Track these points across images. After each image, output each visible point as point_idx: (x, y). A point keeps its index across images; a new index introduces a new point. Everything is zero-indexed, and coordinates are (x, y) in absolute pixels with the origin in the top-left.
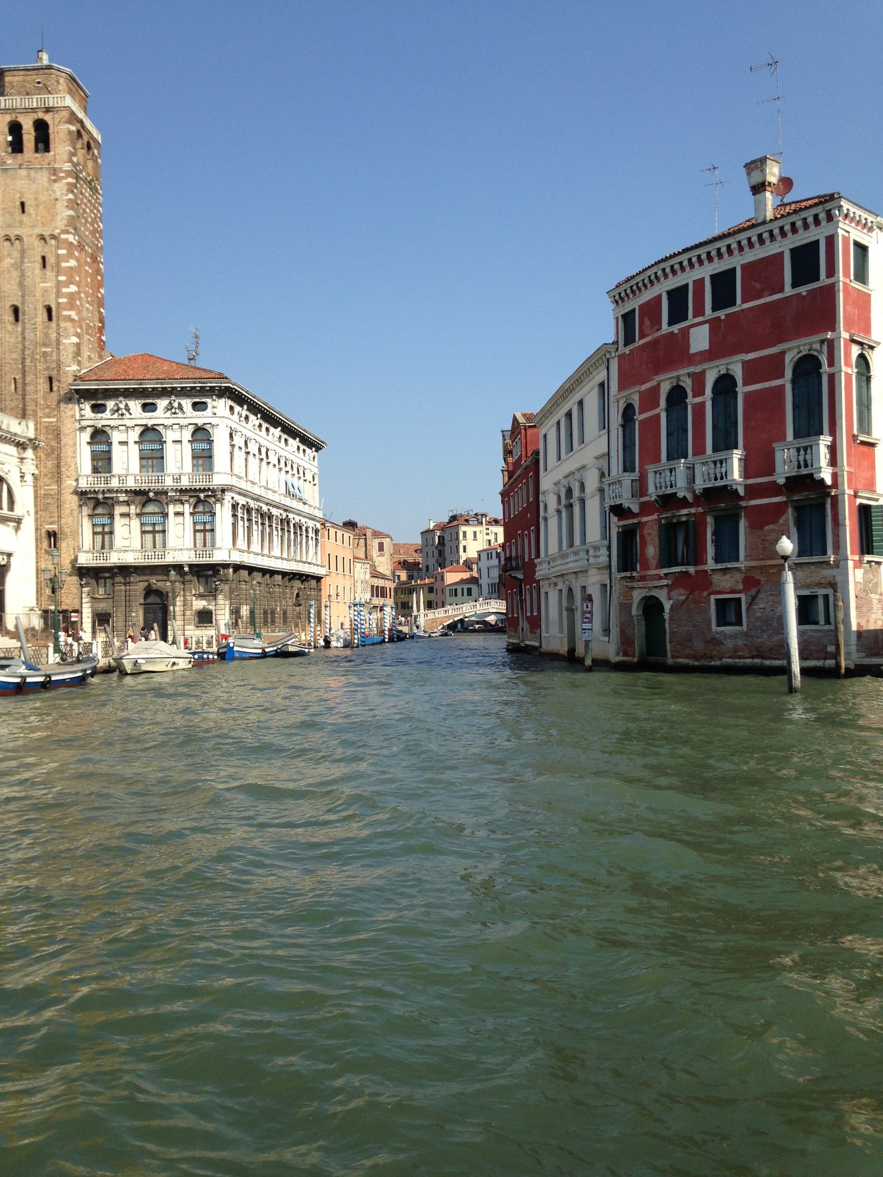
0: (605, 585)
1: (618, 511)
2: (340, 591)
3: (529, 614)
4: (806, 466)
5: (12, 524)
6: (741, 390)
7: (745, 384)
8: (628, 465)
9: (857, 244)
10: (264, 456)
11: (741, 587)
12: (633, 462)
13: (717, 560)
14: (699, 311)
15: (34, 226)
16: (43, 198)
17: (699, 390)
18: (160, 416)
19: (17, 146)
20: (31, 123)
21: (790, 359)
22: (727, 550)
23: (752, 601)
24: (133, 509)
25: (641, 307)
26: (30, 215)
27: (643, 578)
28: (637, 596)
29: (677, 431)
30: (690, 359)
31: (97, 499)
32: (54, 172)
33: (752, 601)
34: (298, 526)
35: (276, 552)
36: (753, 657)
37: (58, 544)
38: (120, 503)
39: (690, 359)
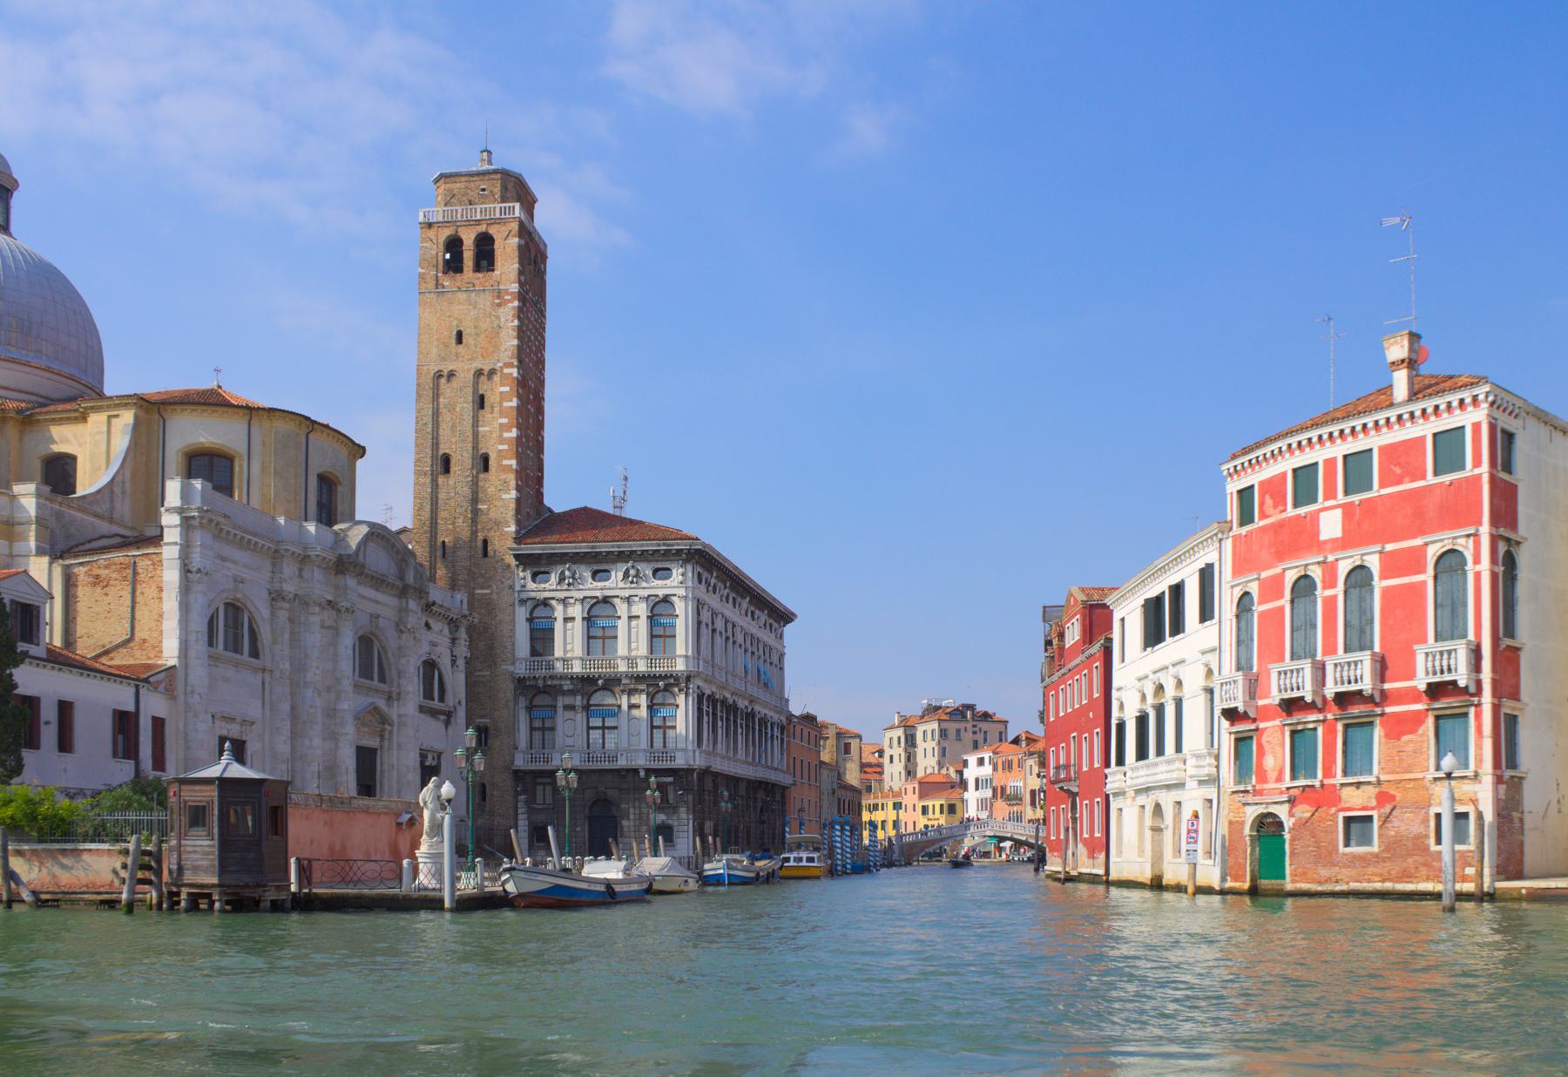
0: (1210, 801)
1: (1231, 715)
2: (805, 805)
3: (1086, 836)
4: (1449, 670)
5: (443, 717)
6: (1379, 585)
7: (1383, 577)
8: (1243, 662)
9: (1503, 431)
10: (730, 633)
11: (1374, 803)
12: (1250, 659)
13: (1345, 773)
14: (1331, 494)
15: (473, 359)
16: (484, 325)
17: (1330, 582)
18: (615, 582)
19: (454, 265)
20: (473, 236)
21: (1433, 552)
22: (1355, 760)
23: (1386, 820)
24: (578, 701)
25: (1262, 484)
26: (468, 346)
27: (1256, 793)
28: (1251, 813)
29: (1303, 627)
30: (1320, 546)
31: (536, 686)
32: (499, 294)
33: (1386, 820)
34: (763, 721)
35: (741, 754)
36: (1383, 881)
37: (490, 742)
38: (564, 693)
39: (1320, 546)
